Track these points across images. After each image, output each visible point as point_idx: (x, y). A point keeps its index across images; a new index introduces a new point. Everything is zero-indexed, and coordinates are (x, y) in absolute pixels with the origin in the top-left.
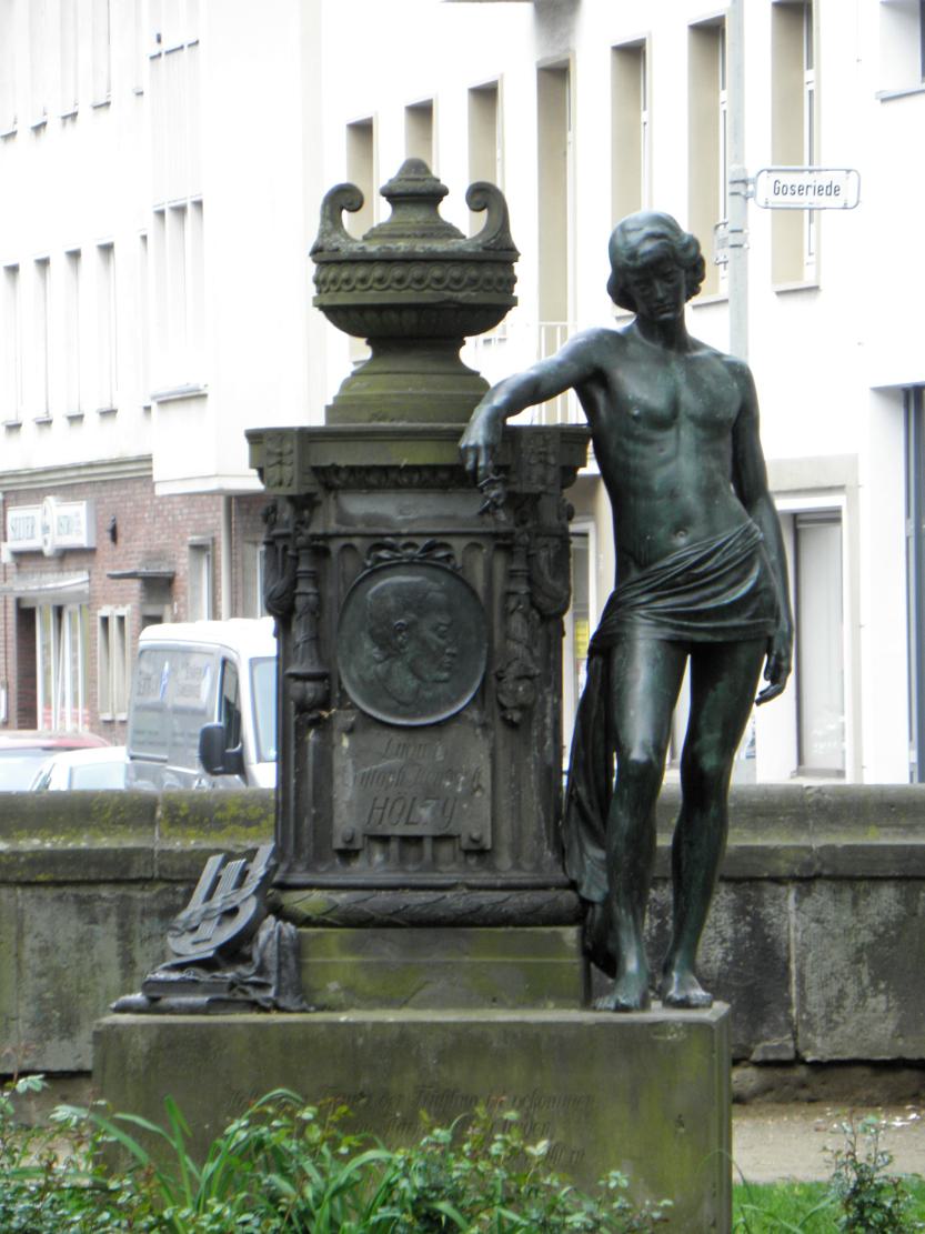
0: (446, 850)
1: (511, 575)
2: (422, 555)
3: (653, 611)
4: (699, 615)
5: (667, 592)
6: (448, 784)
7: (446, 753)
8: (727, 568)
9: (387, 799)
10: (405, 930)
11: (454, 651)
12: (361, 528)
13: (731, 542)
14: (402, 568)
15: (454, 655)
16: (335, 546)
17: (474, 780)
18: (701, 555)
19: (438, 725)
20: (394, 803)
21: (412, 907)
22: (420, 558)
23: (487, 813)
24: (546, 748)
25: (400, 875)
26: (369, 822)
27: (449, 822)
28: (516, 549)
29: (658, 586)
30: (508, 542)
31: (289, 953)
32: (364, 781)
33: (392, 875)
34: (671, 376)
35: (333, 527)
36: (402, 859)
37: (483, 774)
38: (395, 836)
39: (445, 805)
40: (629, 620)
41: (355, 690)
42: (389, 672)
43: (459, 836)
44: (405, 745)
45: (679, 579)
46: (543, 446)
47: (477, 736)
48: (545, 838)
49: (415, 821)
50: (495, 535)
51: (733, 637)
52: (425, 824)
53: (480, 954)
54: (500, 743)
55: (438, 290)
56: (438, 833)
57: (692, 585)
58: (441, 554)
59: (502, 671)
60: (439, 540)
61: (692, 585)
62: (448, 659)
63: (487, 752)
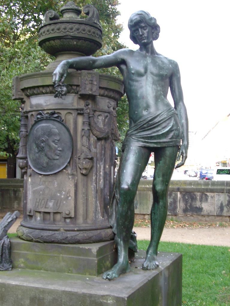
0: (58, 217)
1: (84, 123)
2: (49, 116)
3: (136, 137)
4: (152, 138)
5: (141, 130)
6: (59, 195)
7: (58, 184)
8: (161, 122)
9: (40, 199)
10: (42, 244)
11: (61, 149)
12: (35, 108)
13: (163, 113)
14: (44, 121)
15: (60, 151)
16: (29, 115)
17: (68, 194)
18: (152, 117)
19: (55, 174)
20: (42, 201)
21: (43, 237)
22: (49, 117)
23: (73, 205)
24: (101, 182)
25: (43, 225)
26: (35, 207)
27: (59, 208)
28: (85, 114)
29: (138, 128)
30: (82, 112)
31: (7, 249)
32: (34, 192)
33: (41, 225)
34: (146, 60)
35: (29, 109)
36: (44, 220)
37: (71, 192)
38: (42, 212)
39: (57, 202)
40: (129, 140)
41: (31, 162)
42: (39, 156)
43: (62, 213)
44: (45, 181)
45: (145, 126)
46: (91, 78)
47: (69, 179)
48: (100, 212)
49: (47, 207)
50: (77, 110)
51: (164, 145)
52: (51, 208)
53: (63, 257)
54: (80, 180)
55: (65, 32)
56: (55, 211)
57: (149, 128)
58: (56, 115)
59: (79, 156)
60: (56, 111)
61: (149, 128)
62: (59, 152)
63: (73, 184)
